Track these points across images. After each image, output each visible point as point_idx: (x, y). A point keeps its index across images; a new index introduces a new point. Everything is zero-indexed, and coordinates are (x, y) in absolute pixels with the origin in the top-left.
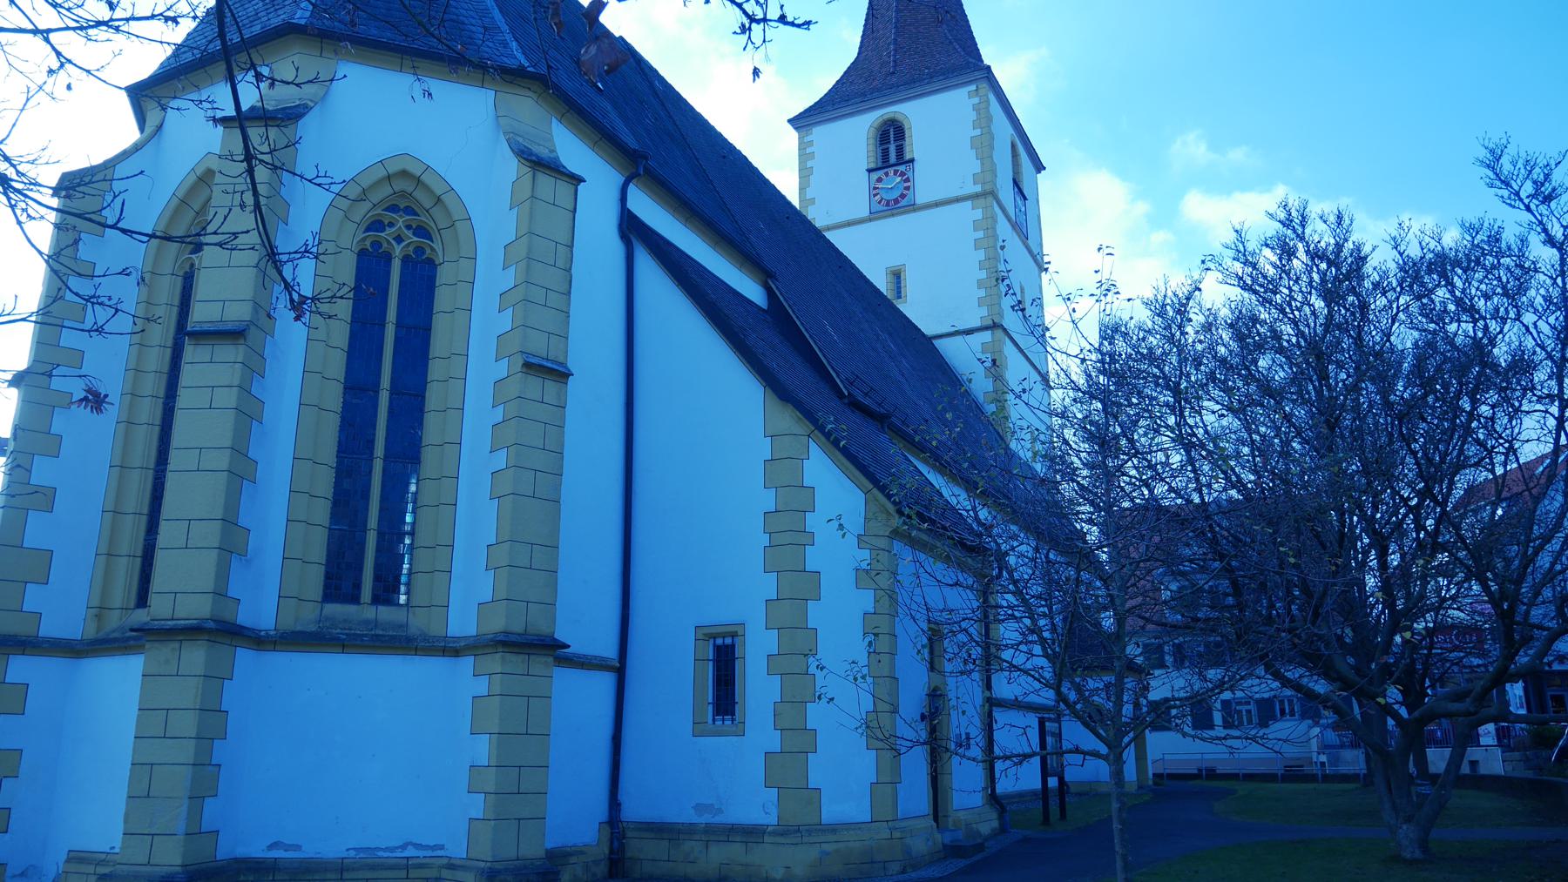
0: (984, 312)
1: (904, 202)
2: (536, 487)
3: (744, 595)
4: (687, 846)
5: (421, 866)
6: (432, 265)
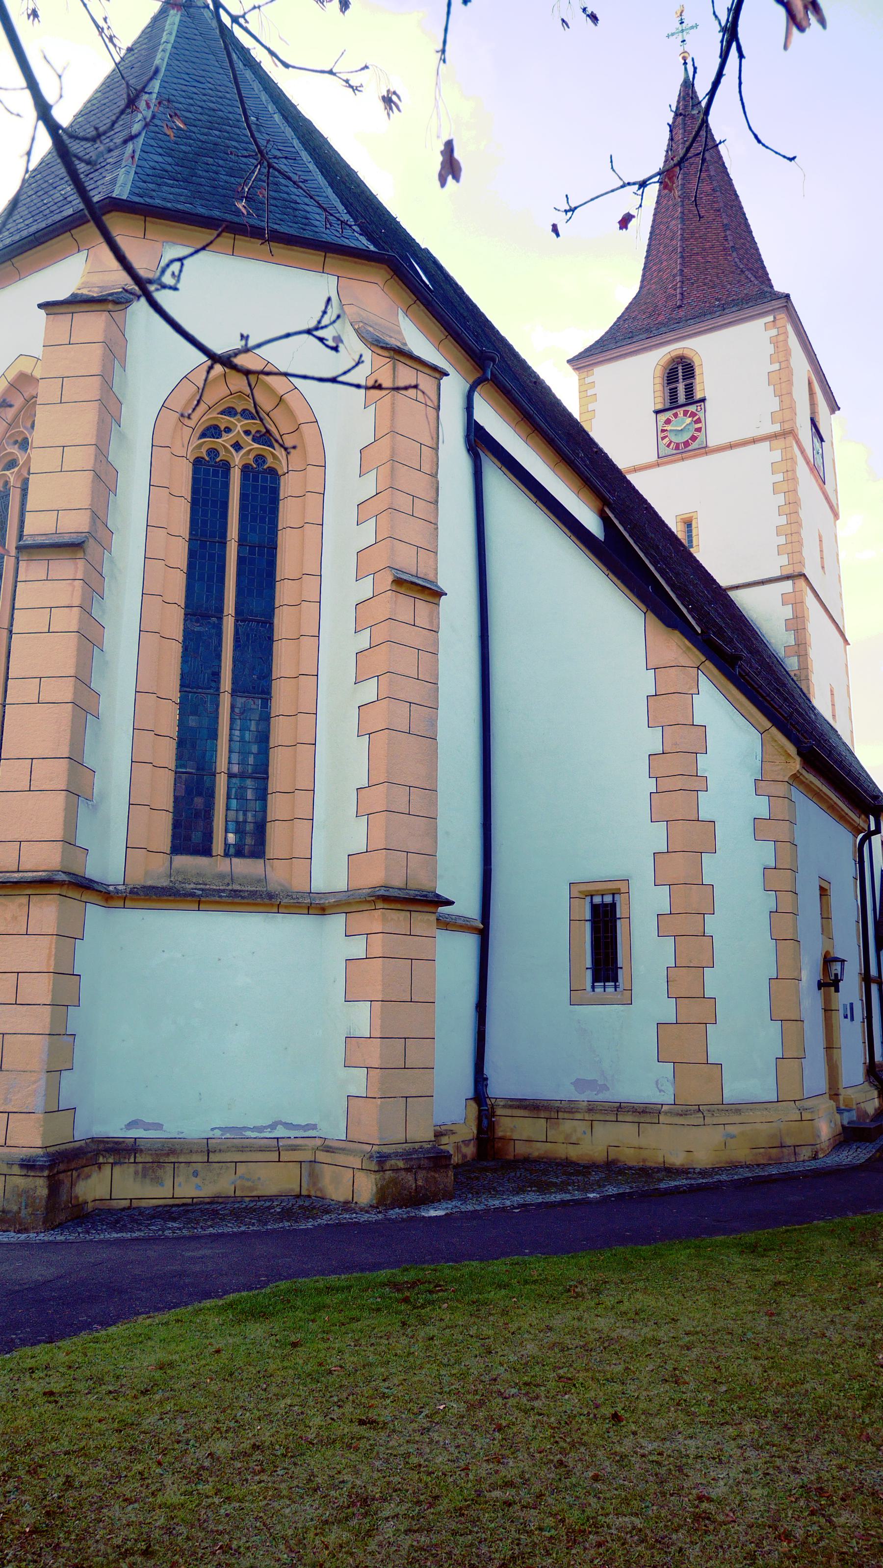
0: (784, 560)
1: (695, 445)
2: (403, 724)
3: (627, 847)
4: (567, 1126)
5: (294, 1148)
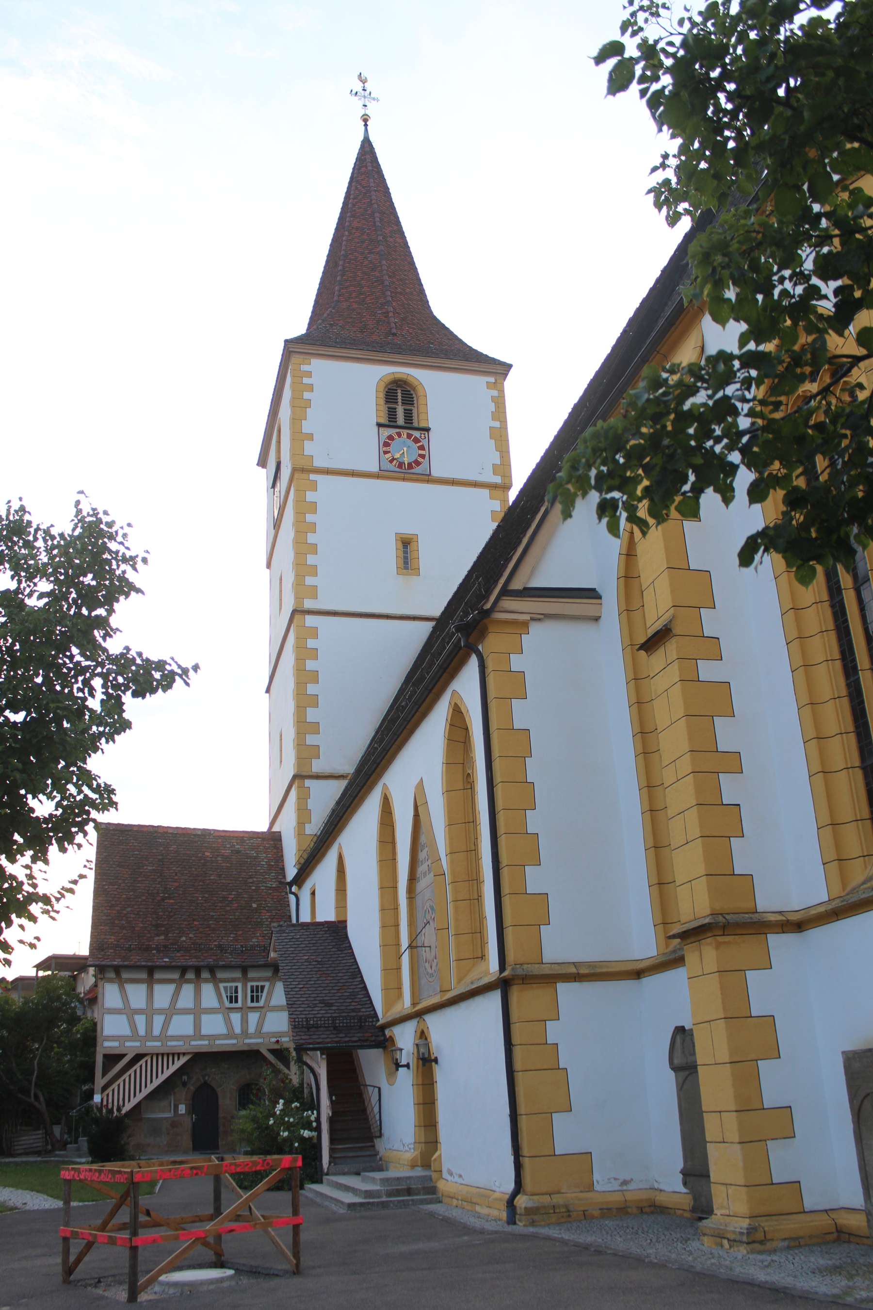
1: (418, 470)
6: (387, 402)
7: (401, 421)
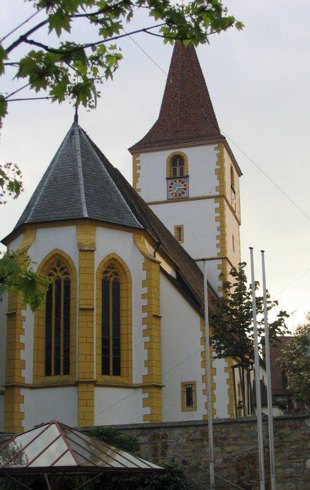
0: (219, 250)
1: (183, 196)
3: (195, 373)
7: (178, 175)
